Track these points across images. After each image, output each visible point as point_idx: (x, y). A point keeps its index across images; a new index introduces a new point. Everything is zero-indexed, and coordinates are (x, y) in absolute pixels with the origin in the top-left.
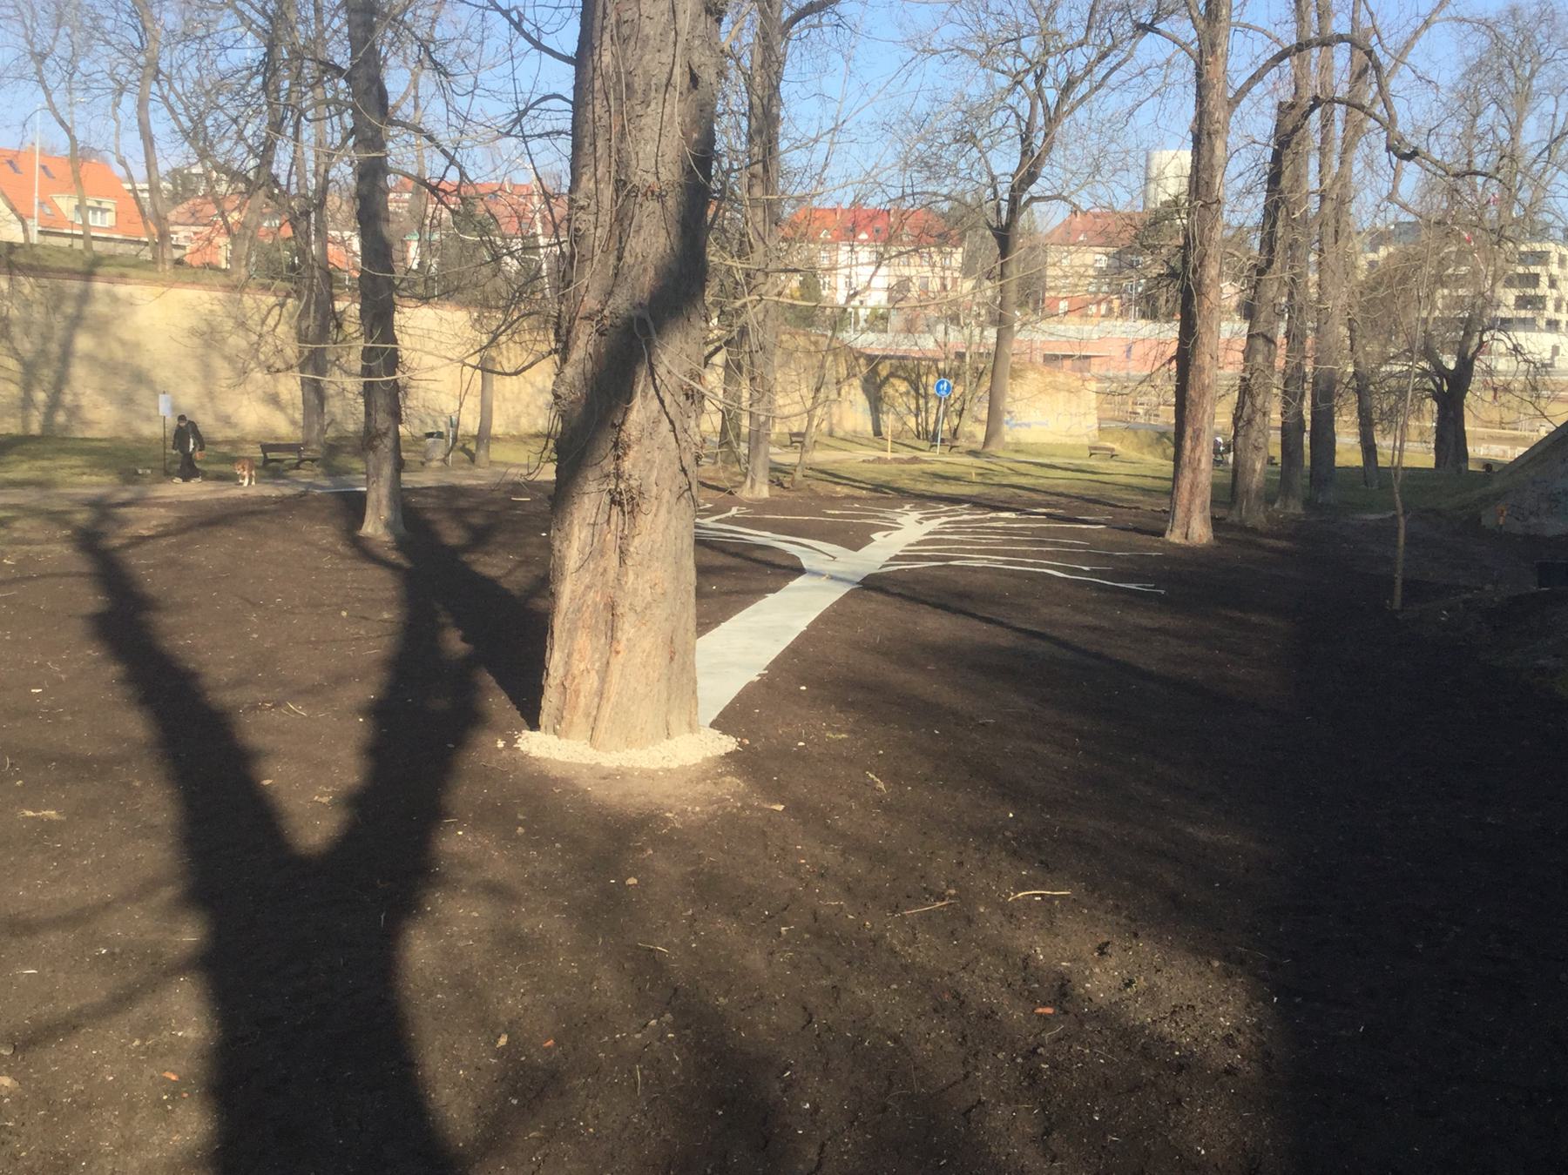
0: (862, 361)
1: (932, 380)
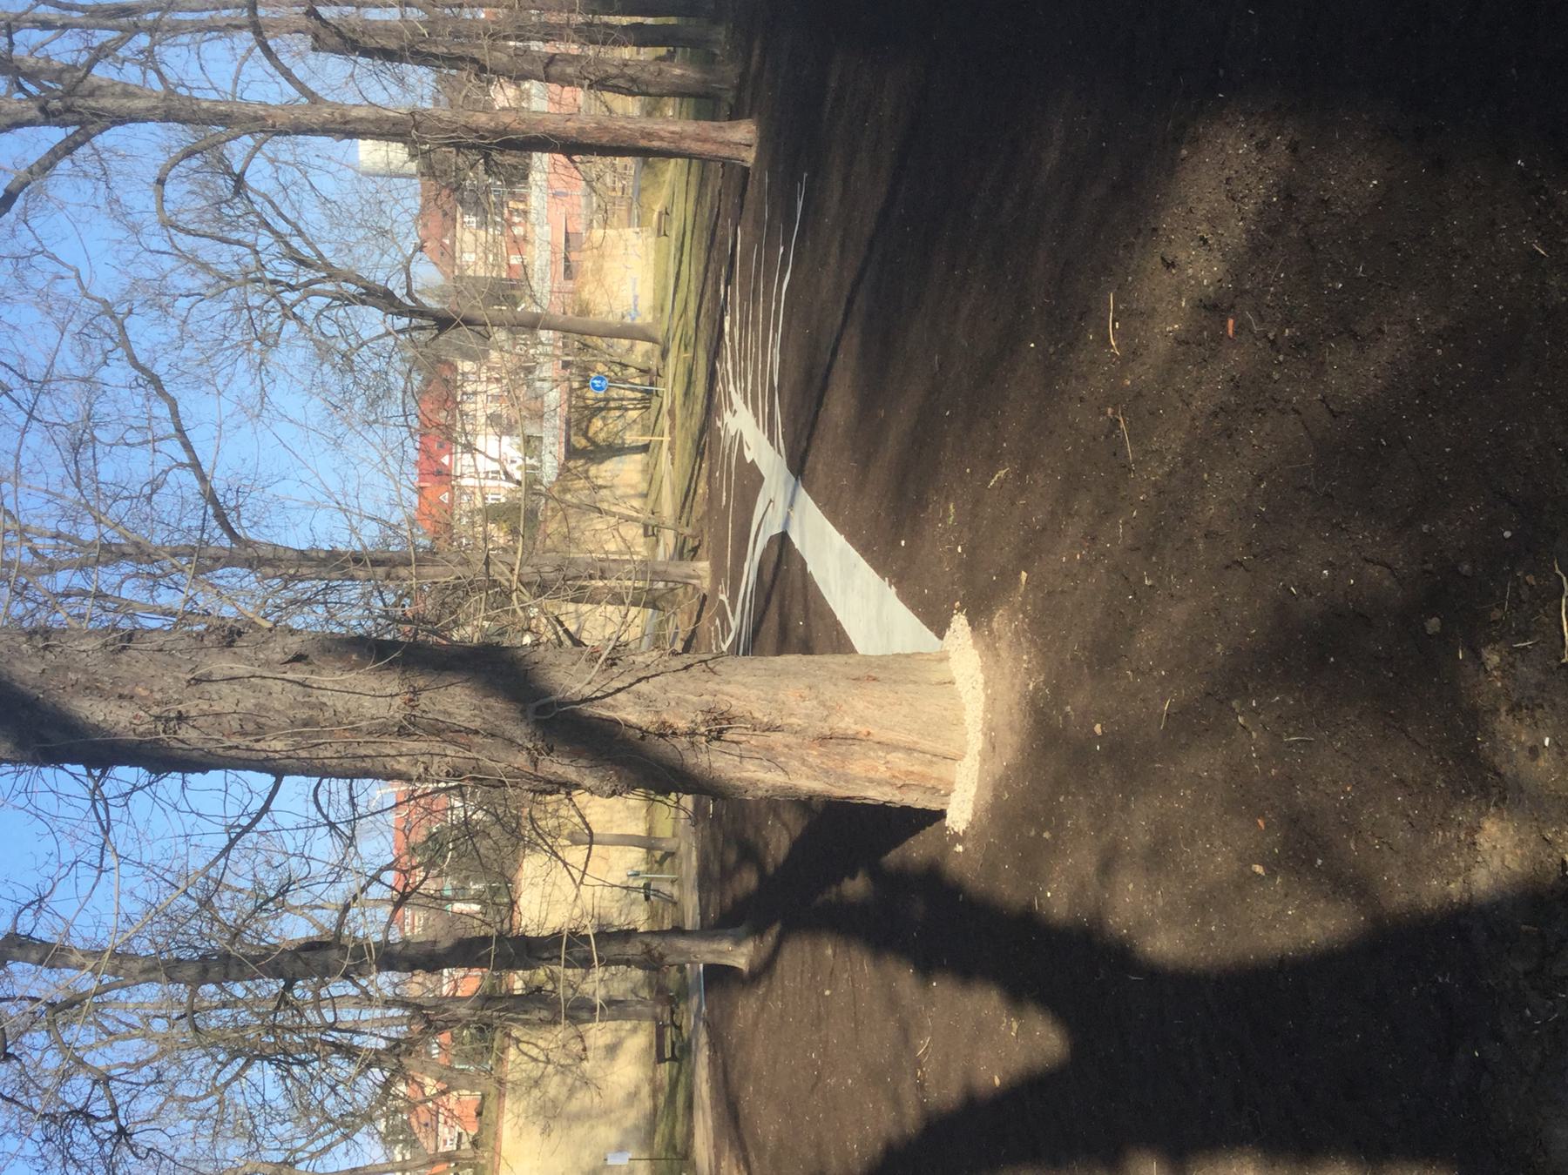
0: (571, 464)
1: (590, 394)
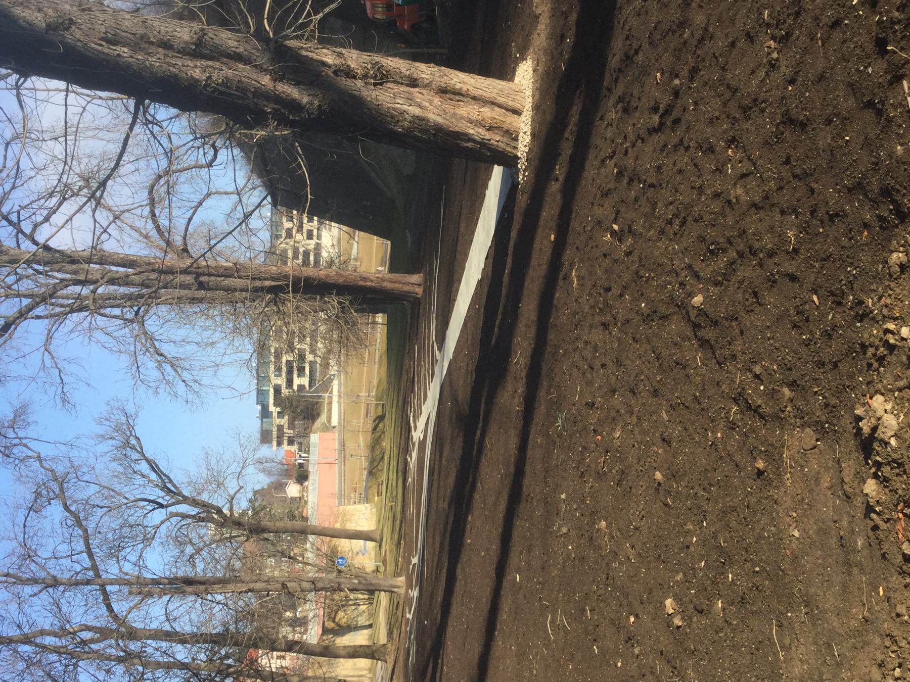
0: (325, 637)
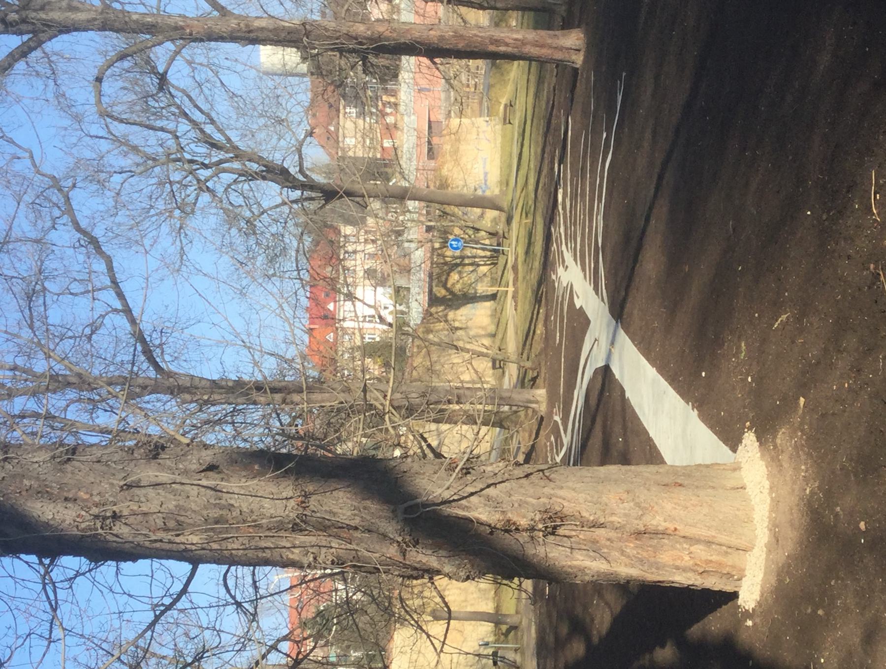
0: (433, 310)
1: (449, 253)
